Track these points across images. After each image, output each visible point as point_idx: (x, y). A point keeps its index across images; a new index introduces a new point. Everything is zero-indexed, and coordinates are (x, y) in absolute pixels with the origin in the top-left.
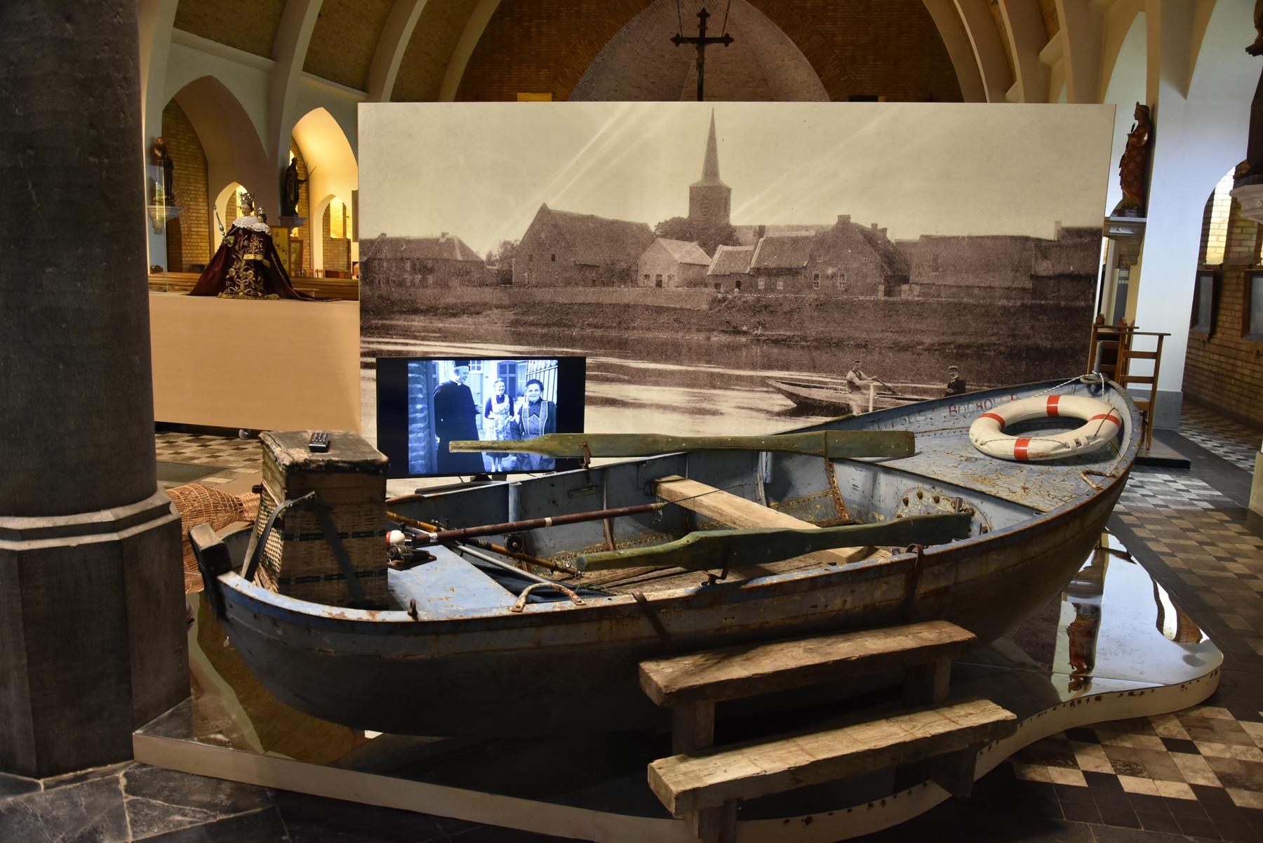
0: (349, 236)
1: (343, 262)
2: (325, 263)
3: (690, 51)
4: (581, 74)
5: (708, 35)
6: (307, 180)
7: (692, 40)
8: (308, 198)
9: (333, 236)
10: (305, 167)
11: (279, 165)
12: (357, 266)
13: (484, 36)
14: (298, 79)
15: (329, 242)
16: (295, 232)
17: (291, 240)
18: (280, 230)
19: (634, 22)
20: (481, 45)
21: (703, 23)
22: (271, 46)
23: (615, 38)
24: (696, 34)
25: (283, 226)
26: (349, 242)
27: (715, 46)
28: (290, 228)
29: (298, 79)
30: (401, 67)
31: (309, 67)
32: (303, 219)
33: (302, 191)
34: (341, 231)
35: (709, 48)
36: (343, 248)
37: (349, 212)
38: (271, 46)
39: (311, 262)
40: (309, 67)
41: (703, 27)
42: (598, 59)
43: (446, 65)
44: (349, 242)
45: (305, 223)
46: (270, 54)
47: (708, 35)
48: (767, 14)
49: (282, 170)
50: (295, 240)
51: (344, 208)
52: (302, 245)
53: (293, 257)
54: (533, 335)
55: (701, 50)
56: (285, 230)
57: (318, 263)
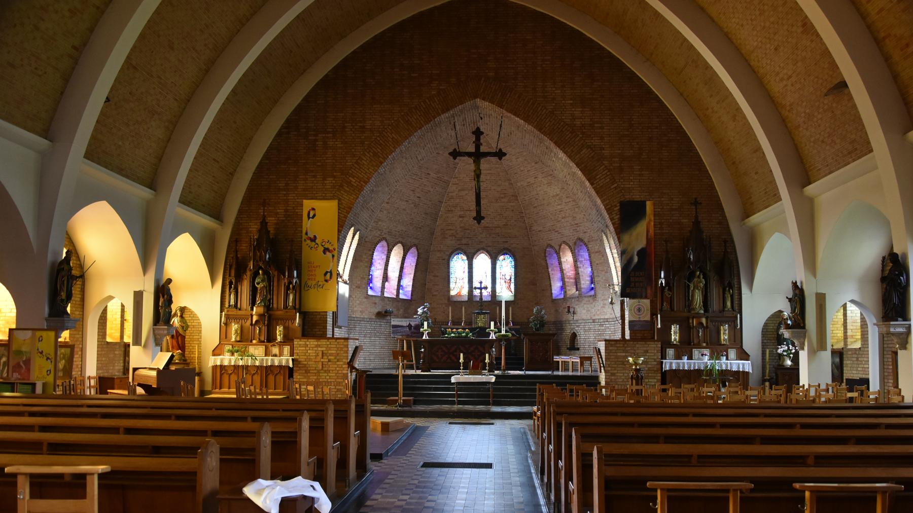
0: (128, 339)
1: (119, 366)
2: (98, 369)
3: (467, 164)
4: (366, 183)
5: (483, 149)
6: (82, 277)
7: (469, 154)
8: (83, 300)
9: (109, 340)
10: (81, 266)
11: (50, 258)
12: (93, 382)
13: (270, 148)
14: (76, 165)
15: (104, 346)
16: (65, 335)
17: (58, 346)
18: (44, 334)
19: (414, 139)
20: (267, 156)
21: (478, 139)
22: (49, 124)
23: (398, 150)
24: (472, 149)
25: (49, 329)
26: (127, 346)
27: (473, 167)
28: (58, 331)
29: (76, 165)
30: (190, 170)
31: (92, 154)
32: (76, 321)
33: (76, 290)
34: (118, 334)
35: (485, 164)
36: (119, 352)
37: (129, 316)
38: (49, 124)
39: (82, 368)
40: (92, 154)
41: (478, 145)
42: (381, 170)
43: (232, 174)
44: (127, 346)
45: (78, 325)
46: (46, 133)
47: (483, 149)
48: (540, 130)
49: (53, 264)
50: (65, 345)
51: (123, 311)
52: (73, 351)
53: (61, 365)
54: (689, 457)
55: (477, 162)
56: (52, 334)
57: (91, 369)
